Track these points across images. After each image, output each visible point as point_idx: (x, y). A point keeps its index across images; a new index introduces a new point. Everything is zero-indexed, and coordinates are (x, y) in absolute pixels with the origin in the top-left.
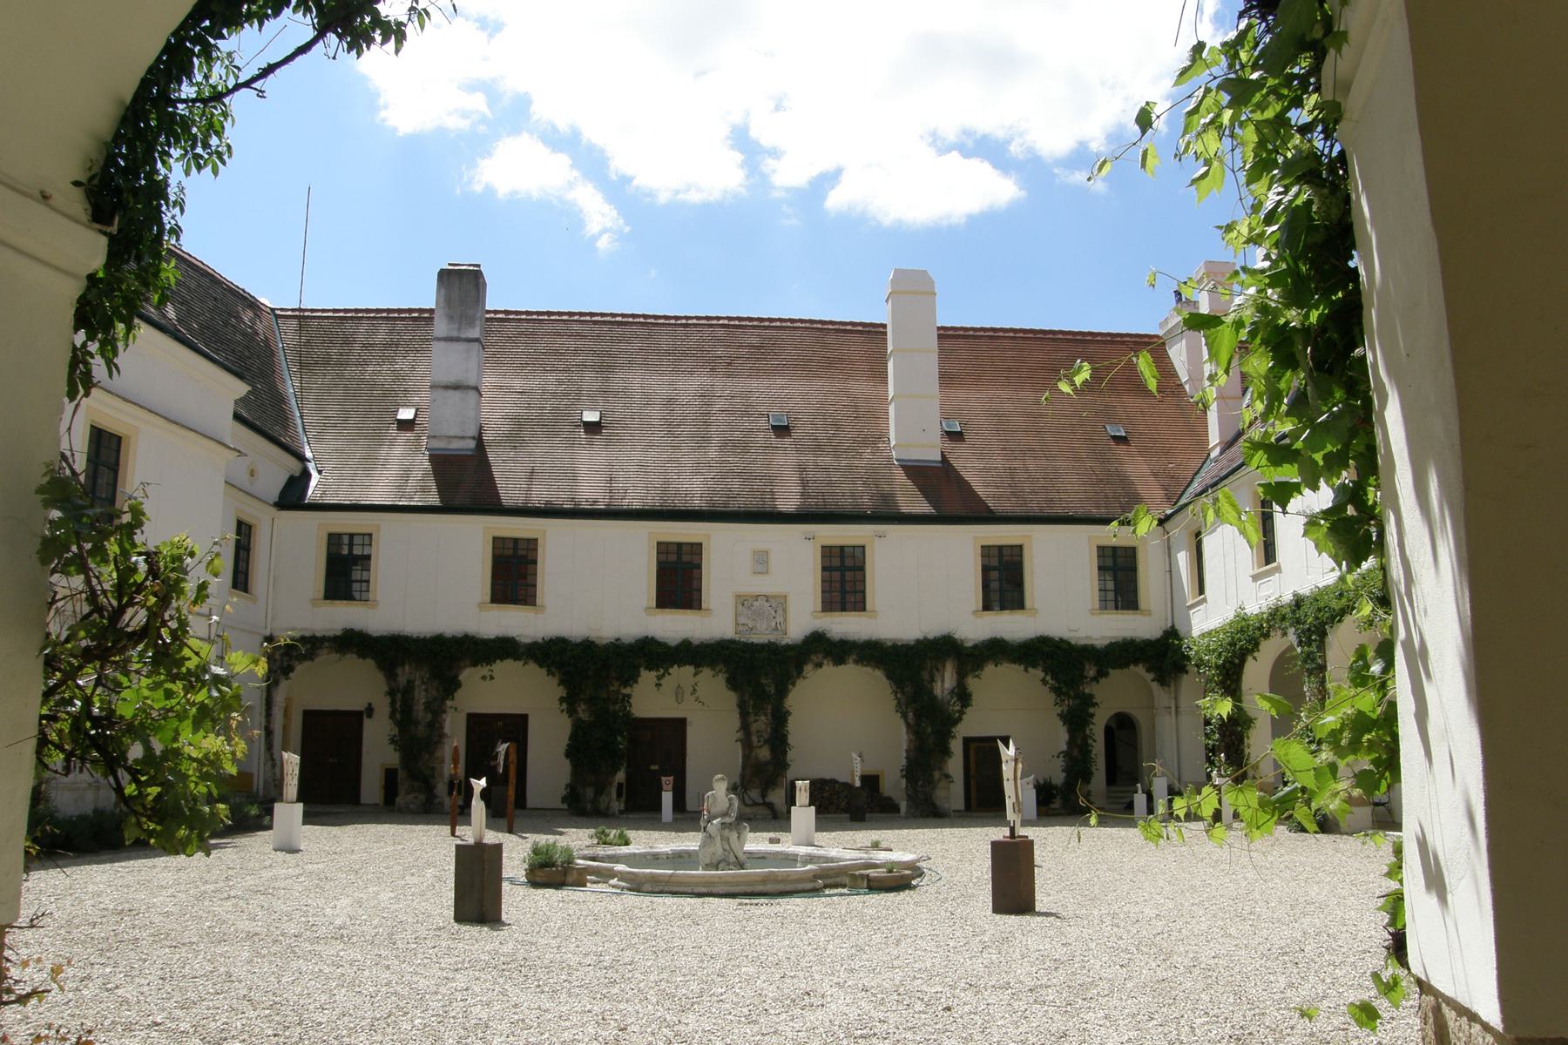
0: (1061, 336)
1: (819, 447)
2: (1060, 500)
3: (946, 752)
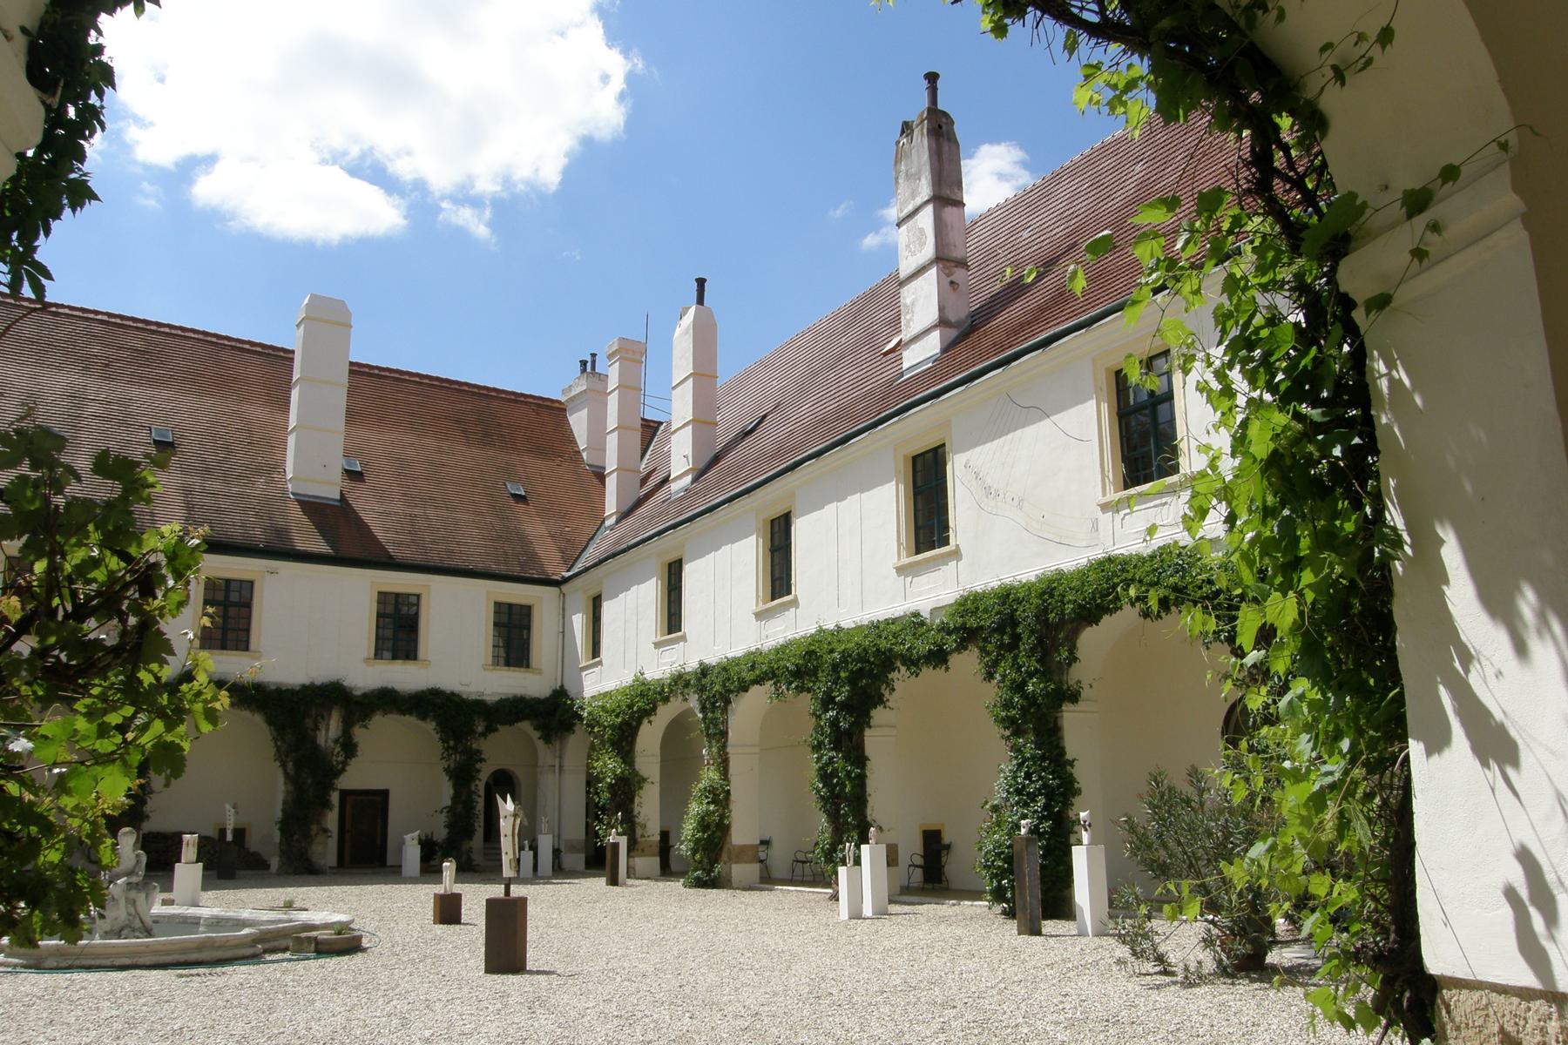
0: (466, 388)
1: (207, 470)
2: (461, 552)
3: (326, 805)
